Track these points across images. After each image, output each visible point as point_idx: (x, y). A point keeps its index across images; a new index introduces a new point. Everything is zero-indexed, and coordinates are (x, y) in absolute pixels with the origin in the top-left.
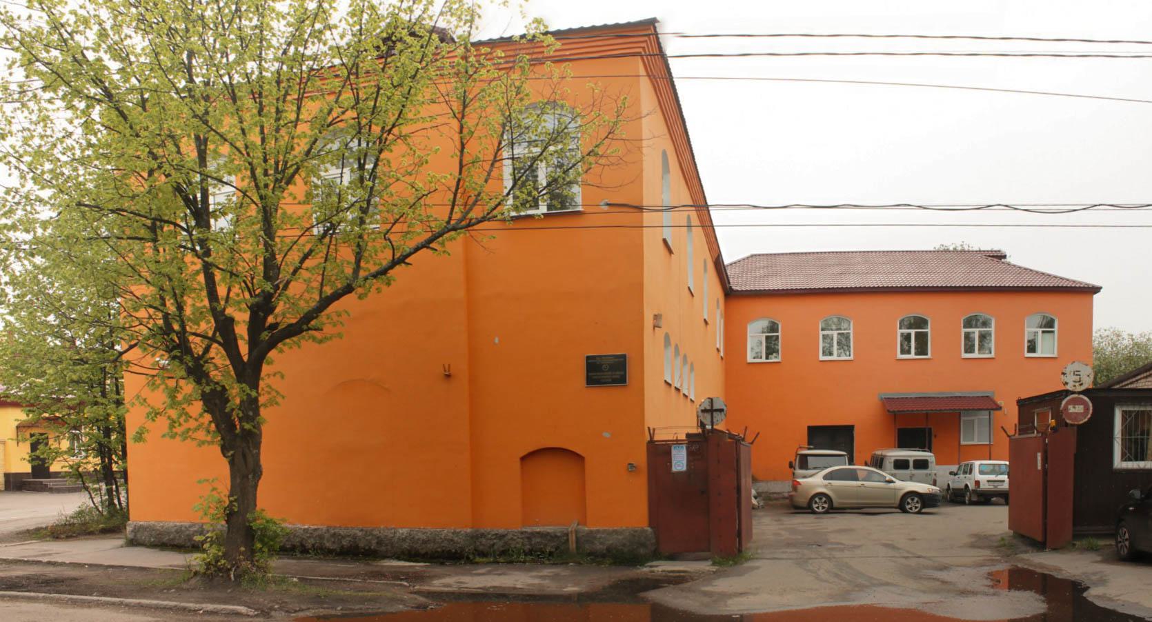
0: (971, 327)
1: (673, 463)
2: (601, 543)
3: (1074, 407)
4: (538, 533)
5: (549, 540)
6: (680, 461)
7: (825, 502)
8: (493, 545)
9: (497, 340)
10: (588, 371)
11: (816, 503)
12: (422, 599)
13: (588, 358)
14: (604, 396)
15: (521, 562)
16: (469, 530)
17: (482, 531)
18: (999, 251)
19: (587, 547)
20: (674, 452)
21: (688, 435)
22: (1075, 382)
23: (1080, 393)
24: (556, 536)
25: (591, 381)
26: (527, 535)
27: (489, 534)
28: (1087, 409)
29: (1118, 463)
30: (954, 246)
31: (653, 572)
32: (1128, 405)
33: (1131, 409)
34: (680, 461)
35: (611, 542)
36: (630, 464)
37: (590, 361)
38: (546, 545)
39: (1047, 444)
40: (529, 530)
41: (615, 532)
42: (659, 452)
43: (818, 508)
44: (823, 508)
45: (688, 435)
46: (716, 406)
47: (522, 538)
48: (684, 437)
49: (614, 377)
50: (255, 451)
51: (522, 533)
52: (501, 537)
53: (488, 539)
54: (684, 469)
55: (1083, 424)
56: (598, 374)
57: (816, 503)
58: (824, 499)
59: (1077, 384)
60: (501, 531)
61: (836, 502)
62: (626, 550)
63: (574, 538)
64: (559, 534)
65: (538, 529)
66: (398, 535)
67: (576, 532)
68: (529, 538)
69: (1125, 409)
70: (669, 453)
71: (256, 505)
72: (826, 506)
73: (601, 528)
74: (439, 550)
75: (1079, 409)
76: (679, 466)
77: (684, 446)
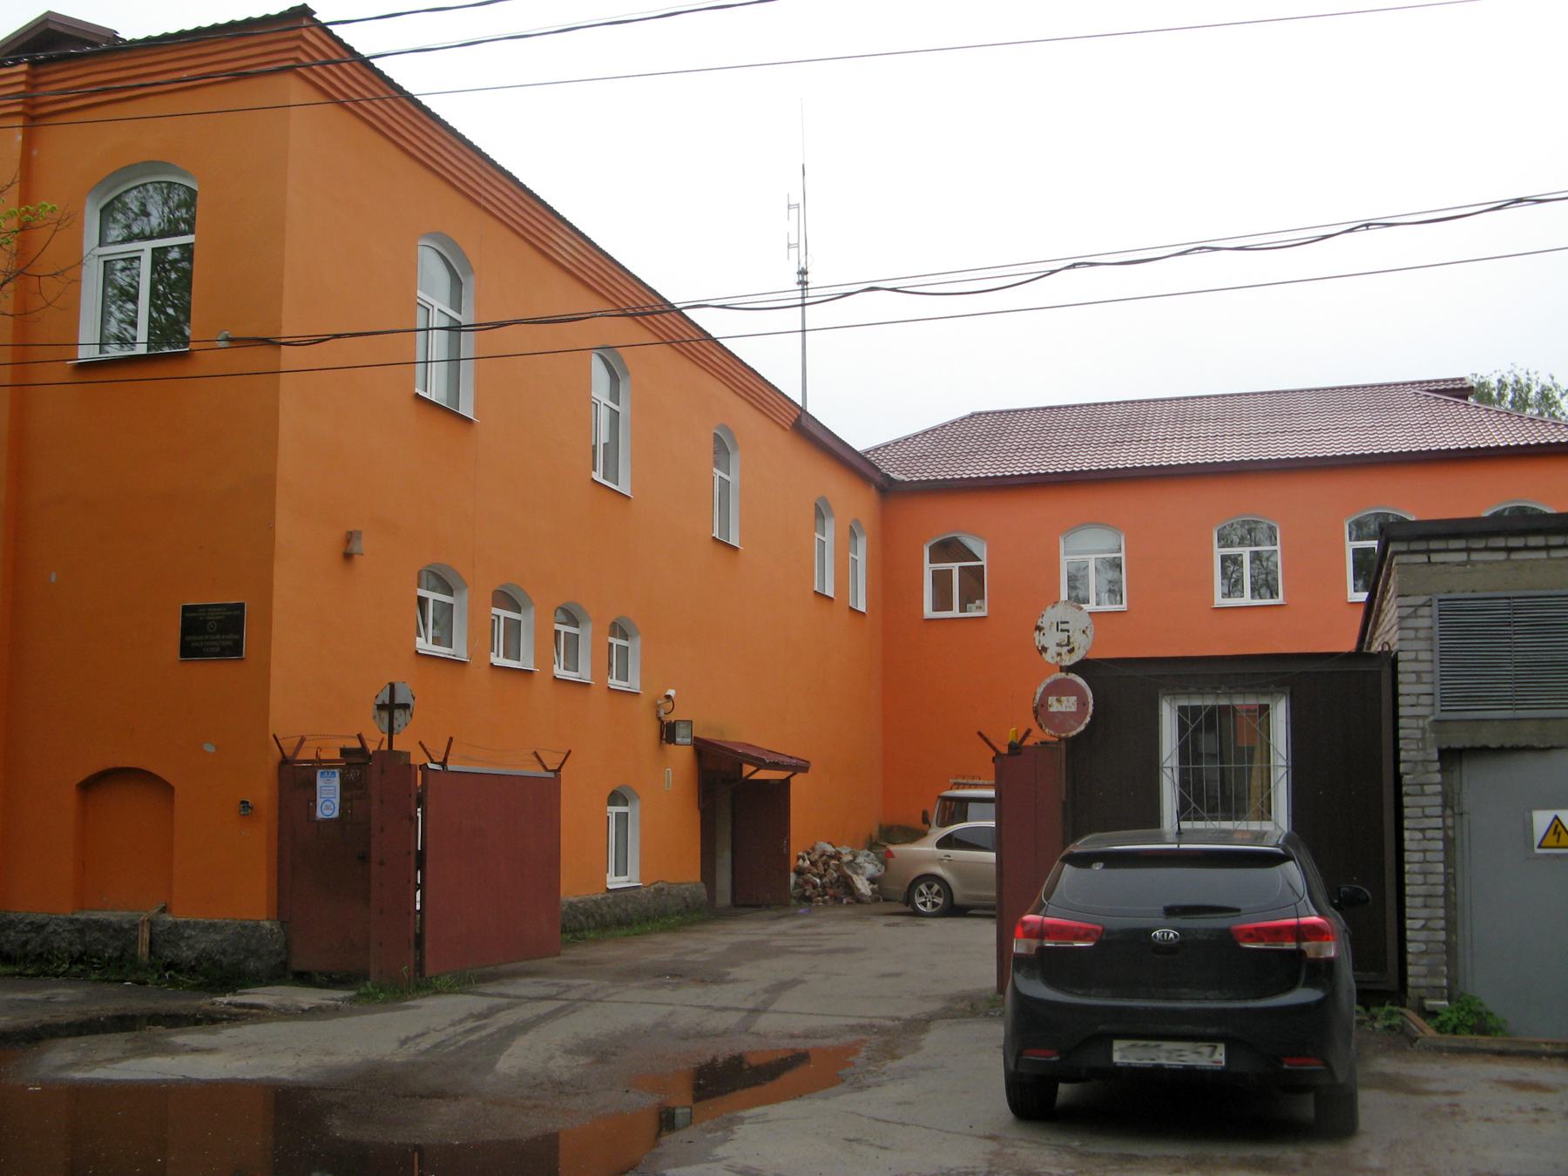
0: (1231, 545)
2: (191, 947)
3: (1059, 701)
4: (96, 922)
5: (112, 937)
6: (328, 798)
7: (938, 894)
8: (26, 943)
9: (53, 578)
11: (921, 894)
13: (186, 609)
14: (210, 674)
15: (27, 975)
17: (12, 916)
18: (1462, 379)
19: (168, 953)
20: (320, 782)
21: (344, 752)
22: (1058, 645)
23: (1068, 669)
24: (122, 929)
25: (188, 651)
26: (78, 926)
27: (21, 921)
28: (1082, 703)
30: (1498, 376)
31: (214, 1004)
34: (328, 798)
36: (243, 802)
37: (187, 615)
38: (106, 946)
39: (347, 764)
40: (81, 916)
43: (924, 904)
44: (934, 905)
46: (399, 700)
47: (69, 931)
49: (224, 643)
51: (71, 921)
52: (38, 928)
53: (18, 932)
54: (336, 814)
55: (1074, 737)
56: (201, 638)
57: (921, 894)
58: (936, 887)
59: (1065, 649)
60: (39, 918)
61: (959, 895)
62: (226, 961)
63: (146, 936)
67: (152, 923)
68: (81, 932)
69: (1185, 702)
70: (312, 784)
72: (939, 901)
73: (191, 919)
75: (1068, 704)
76: (327, 808)
77: (337, 772)
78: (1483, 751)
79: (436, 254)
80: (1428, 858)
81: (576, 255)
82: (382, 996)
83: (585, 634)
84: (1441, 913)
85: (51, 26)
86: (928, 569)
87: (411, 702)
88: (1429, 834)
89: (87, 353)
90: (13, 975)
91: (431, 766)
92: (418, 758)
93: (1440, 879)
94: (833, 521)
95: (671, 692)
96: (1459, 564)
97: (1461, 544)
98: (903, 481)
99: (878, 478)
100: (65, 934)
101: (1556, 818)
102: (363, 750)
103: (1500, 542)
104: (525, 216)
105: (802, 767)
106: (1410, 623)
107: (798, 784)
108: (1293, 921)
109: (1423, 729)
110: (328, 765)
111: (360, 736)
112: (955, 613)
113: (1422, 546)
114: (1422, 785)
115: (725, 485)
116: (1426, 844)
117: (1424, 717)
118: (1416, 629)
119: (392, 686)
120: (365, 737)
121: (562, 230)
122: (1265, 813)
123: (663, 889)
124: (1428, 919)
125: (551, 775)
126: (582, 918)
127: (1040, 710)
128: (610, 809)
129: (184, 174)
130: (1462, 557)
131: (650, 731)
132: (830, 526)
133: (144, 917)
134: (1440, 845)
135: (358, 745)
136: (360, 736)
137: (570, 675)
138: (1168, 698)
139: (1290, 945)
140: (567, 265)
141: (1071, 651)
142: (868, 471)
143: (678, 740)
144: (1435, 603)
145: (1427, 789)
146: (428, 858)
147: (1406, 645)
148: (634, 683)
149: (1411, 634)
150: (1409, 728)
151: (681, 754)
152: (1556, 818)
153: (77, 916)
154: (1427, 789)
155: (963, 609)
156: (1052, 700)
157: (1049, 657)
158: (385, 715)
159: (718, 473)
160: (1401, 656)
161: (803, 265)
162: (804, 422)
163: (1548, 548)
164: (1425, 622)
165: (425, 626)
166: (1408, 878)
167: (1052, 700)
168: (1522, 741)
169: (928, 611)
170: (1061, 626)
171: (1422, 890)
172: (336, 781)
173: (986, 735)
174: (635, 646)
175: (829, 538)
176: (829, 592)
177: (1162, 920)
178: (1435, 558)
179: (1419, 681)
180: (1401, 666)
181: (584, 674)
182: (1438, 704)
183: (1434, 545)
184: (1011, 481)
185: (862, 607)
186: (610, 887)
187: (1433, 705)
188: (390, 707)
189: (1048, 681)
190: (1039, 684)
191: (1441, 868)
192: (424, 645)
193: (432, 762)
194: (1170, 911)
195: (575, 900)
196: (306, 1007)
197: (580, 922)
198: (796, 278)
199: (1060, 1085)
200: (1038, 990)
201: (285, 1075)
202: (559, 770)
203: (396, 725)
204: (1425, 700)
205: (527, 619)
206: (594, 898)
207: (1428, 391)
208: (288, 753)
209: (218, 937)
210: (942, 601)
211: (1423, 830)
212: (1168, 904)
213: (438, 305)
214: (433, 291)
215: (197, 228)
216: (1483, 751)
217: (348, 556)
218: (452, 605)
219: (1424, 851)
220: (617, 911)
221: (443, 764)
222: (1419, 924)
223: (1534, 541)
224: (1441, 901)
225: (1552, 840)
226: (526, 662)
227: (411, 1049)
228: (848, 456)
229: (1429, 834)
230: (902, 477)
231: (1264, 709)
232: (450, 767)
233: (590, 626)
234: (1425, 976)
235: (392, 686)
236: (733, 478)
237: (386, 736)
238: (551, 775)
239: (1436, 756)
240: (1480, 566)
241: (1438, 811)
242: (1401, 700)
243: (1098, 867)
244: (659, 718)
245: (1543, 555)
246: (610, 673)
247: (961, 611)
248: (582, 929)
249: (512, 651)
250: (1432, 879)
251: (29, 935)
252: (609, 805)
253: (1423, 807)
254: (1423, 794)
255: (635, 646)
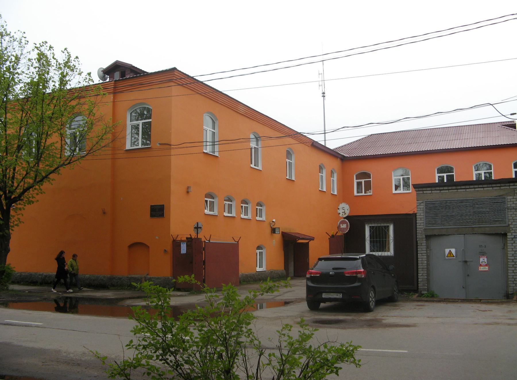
1: (182, 250)
3: (342, 225)
4: (133, 277)
6: (184, 249)
8: (117, 282)
9: (122, 199)
10: (151, 212)
12: (300, 313)
13: (151, 206)
14: (157, 221)
16: (109, 276)
20: (182, 245)
21: (187, 238)
23: (344, 218)
25: (152, 216)
27: (116, 277)
28: (347, 226)
29: (391, 253)
32: (371, 223)
33: (373, 225)
34: (184, 249)
35: (156, 282)
40: (130, 276)
41: (158, 278)
42: (176, 244)
45: (187, 238)
46: (199, 226)
48: (185, 239)
50: (6, 243)
51: (127, 277)
52: (120, 279)
54: (185, 252)
64: (139, 278)
65: (133, 276)
66: (85, 277)
71: (6, 262)
73: (154, 277)
74: (99, 284)
77: (185, 243)
78: (435, 236)
79: (210, 118)
80: (421, 259)
81: (245, 111)
82: (196, 293)
83: (249, 206)
84: (426, 272)
85: (117, 64)
86: (355, 181)
87: (202, 227)
88: (423, 254)
89: (128, 147)
90: (115, 289)
91: (206, 241)
92: (203, 239)
93: (425, 264)
94: (325, 170)
95: (274, 220)
96: (429, 193)
97: (430, 189)
98: (348, 157)
99: (340, 156)
100: (126, 280)
101: (450, 250)
102: (191, 238)
103: (438, 188)
104: (231, 103)
105: (312, 239)
106: (419, 207)
107: (311, 243)
108: (355, 271)
109: (422, 231)
110: (183, 241)
111: (190, 235)
112: (363, 194)
113: (421, 189)
114: (422, 243)
115: (290, 164)
116: (422, 257)
117: (422, 228)
118: (420, 208)
119: (197, 223)
120: (191, 235)
121: (240, 105)
122: (389, 251)
123: (272, 272)
124: (423, 274)
125: (236, 243)
126: (249, 278)
127: (339, 227)
128: (257, 251)
129: (148, 105)
130: (430, 192)
131: (269, 230)
132: (324, 171)
133: (143, 276)
134: (425, 257)
135: (190, 237)
136: (190, 235)
137: (246, 217)
138: (367, 224)
139: (355, 275)
140: (243, 113)
141: (345, 214)
142: (337, 155)
143: (276, 232)
144: (424, 202)
145: (423, 244)
146: (206, 262)
147: (418, 212)
148: (264, 218)
149: (419, 209)
150: (419, 231)
151: (278, 236)
152: (450, 250)
153: (129, 276)
154: (423, 244)
155: (365, 193)
156: (341, 225)
157: (341, 215)
158: (196, 230)
159: (288, 160)
160: (417, 214)
161: (323, 91)
162: (314, 144)
163: (449, 190)
164: (422, 207)
165: (207, 207)
166: (419, 265)
167: (341, 225)
168: (443, 233)
169: (355, 193)
170: (343, 209)
171: (421, 267)
172: (185, 245)
173: (328, 233)
174: (264, 209)
175: (324, 175)
176: (325, 190)
177: (332, 271)
178: (425, 192)
179: (421, 220)
180: (417, 217)
181: (249, 216)
182: (425, 225)
183: (424, 189)
184: (378, 156)
185: (336, 193)
186: (257, 271)
187: (508, 217)
188: (197, 228)
189: (340, 221)
190: (338, 221)
191: (426, 262)
192: (207, 212)
193: (207, 240)
194: (333, 269)
195: (247, 274)
196: (179, 295)
197: (249, 279)
198: (322, 95)
199: (321, 304)
200: (310, 284)
201: (173, 305)
202: (238, 241)
203: (198, 232)
204: (422, 224)
205: (233, 204)
206: (253, 273)
207: (503, 125)
208: (174, 239)
209: (160, 280)
210: (359, 190)
211: (422, 254)
212: (333, 267)
213: (209, 129)
214: (208, 127)
215: (152, 118)
216: (435, 236)
217: (188, 192)
218: (214, 202)
219: (422, 258)
220: (259, 277)
221: (209, 241)
222: (421, 275)
223: (445, 188)
224: (426, 270)
225: (449, 255)
226: (234, 214)
227: (199, 301)
228: (330, 152)
229: (423, 254)
230: (347, 155)
231: (388, 226)
232: (211, 241)
233: (251, 204)
234: (422, 286)
235: (197, 223)
236: (293, 161)
237: (196, 235)
238: (236, 243)
239: (424, 237)
240: (434, 194)
241: (425, 249)
242: (417, 224)
243: (323, 261)
244: (271, 227)
245: (447, 191)
246: (257, 216)
247: (365, 193)
248: (249, 281)
249: (230, 212)
250: (424, 265)
251: (119, 280)
252: (257, 250)
253: (422, 248)
254: (422, 245)
255: (264, 209)
